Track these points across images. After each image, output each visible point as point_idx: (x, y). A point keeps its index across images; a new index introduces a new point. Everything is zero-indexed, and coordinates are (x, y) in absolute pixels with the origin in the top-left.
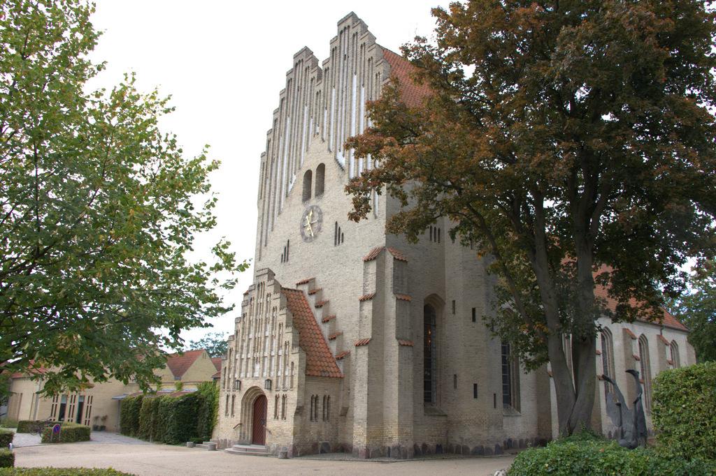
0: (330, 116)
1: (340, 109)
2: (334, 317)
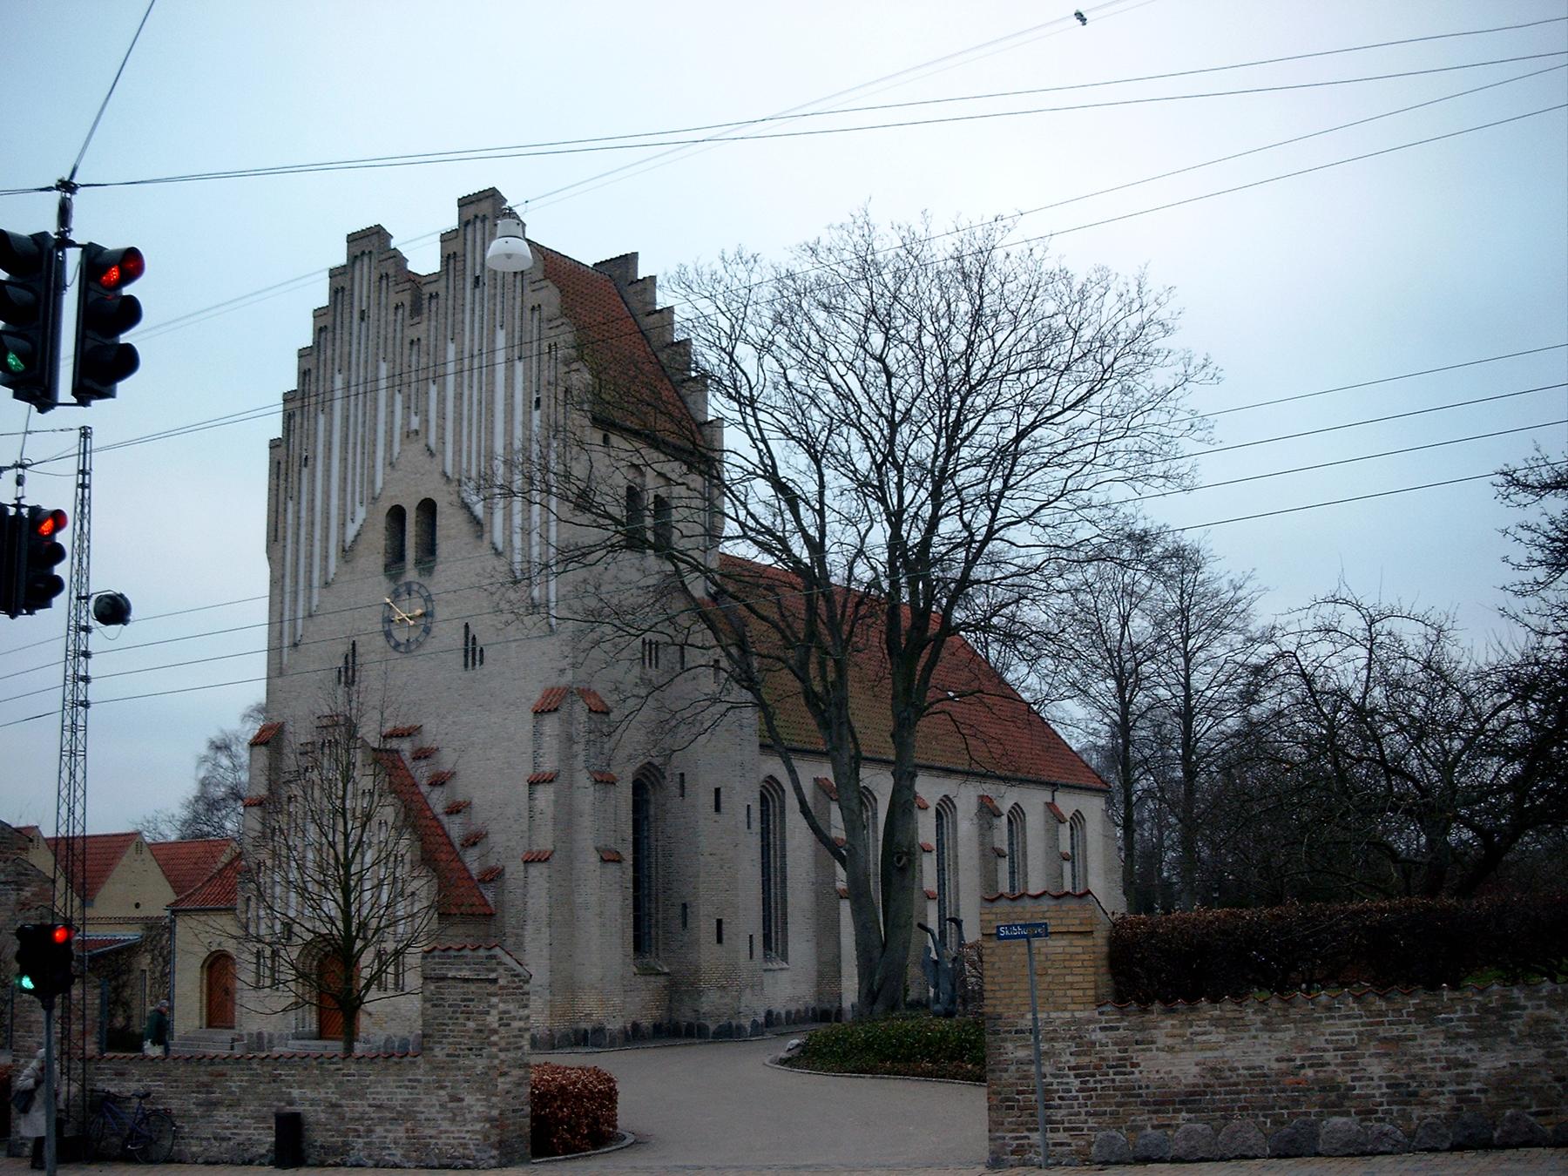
0: (442, 400)
1: (466, 393)
2: (468, 805)
